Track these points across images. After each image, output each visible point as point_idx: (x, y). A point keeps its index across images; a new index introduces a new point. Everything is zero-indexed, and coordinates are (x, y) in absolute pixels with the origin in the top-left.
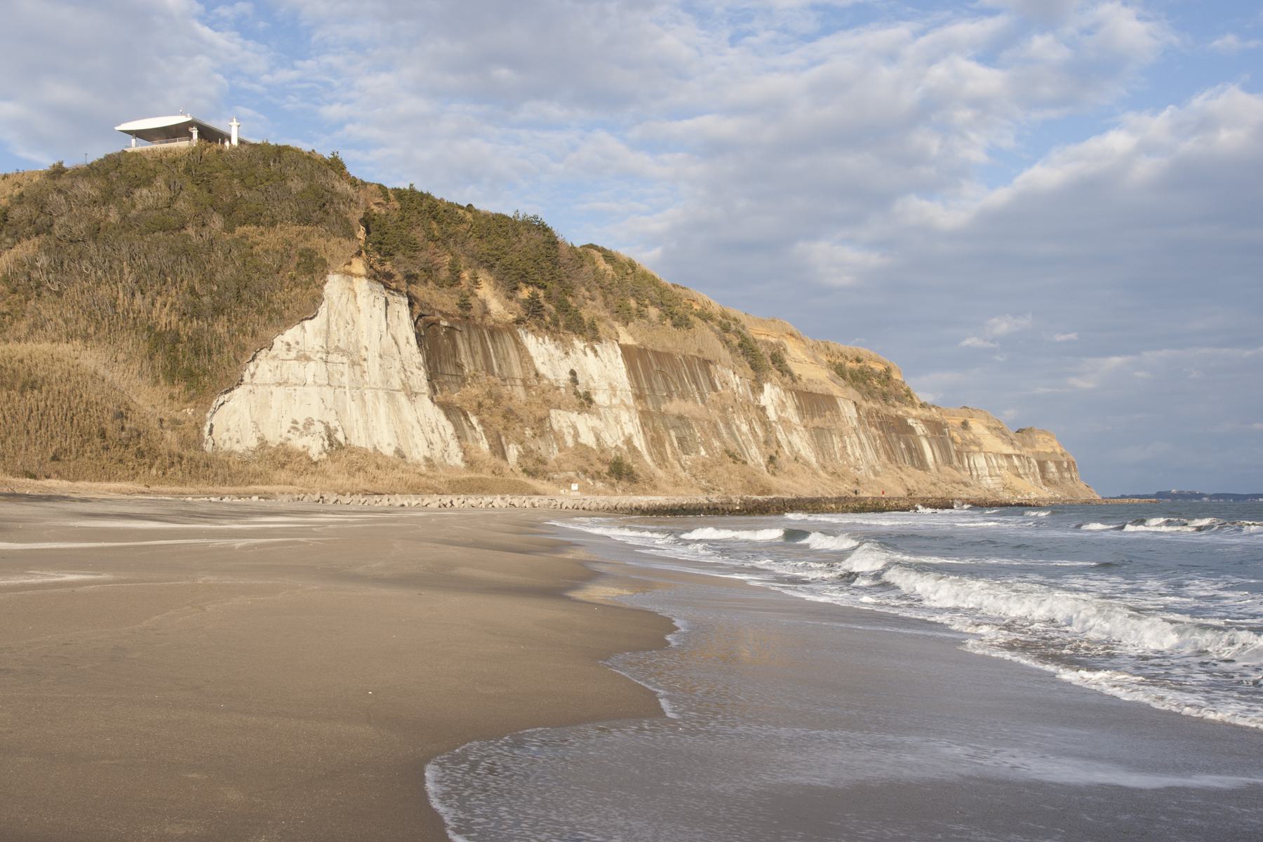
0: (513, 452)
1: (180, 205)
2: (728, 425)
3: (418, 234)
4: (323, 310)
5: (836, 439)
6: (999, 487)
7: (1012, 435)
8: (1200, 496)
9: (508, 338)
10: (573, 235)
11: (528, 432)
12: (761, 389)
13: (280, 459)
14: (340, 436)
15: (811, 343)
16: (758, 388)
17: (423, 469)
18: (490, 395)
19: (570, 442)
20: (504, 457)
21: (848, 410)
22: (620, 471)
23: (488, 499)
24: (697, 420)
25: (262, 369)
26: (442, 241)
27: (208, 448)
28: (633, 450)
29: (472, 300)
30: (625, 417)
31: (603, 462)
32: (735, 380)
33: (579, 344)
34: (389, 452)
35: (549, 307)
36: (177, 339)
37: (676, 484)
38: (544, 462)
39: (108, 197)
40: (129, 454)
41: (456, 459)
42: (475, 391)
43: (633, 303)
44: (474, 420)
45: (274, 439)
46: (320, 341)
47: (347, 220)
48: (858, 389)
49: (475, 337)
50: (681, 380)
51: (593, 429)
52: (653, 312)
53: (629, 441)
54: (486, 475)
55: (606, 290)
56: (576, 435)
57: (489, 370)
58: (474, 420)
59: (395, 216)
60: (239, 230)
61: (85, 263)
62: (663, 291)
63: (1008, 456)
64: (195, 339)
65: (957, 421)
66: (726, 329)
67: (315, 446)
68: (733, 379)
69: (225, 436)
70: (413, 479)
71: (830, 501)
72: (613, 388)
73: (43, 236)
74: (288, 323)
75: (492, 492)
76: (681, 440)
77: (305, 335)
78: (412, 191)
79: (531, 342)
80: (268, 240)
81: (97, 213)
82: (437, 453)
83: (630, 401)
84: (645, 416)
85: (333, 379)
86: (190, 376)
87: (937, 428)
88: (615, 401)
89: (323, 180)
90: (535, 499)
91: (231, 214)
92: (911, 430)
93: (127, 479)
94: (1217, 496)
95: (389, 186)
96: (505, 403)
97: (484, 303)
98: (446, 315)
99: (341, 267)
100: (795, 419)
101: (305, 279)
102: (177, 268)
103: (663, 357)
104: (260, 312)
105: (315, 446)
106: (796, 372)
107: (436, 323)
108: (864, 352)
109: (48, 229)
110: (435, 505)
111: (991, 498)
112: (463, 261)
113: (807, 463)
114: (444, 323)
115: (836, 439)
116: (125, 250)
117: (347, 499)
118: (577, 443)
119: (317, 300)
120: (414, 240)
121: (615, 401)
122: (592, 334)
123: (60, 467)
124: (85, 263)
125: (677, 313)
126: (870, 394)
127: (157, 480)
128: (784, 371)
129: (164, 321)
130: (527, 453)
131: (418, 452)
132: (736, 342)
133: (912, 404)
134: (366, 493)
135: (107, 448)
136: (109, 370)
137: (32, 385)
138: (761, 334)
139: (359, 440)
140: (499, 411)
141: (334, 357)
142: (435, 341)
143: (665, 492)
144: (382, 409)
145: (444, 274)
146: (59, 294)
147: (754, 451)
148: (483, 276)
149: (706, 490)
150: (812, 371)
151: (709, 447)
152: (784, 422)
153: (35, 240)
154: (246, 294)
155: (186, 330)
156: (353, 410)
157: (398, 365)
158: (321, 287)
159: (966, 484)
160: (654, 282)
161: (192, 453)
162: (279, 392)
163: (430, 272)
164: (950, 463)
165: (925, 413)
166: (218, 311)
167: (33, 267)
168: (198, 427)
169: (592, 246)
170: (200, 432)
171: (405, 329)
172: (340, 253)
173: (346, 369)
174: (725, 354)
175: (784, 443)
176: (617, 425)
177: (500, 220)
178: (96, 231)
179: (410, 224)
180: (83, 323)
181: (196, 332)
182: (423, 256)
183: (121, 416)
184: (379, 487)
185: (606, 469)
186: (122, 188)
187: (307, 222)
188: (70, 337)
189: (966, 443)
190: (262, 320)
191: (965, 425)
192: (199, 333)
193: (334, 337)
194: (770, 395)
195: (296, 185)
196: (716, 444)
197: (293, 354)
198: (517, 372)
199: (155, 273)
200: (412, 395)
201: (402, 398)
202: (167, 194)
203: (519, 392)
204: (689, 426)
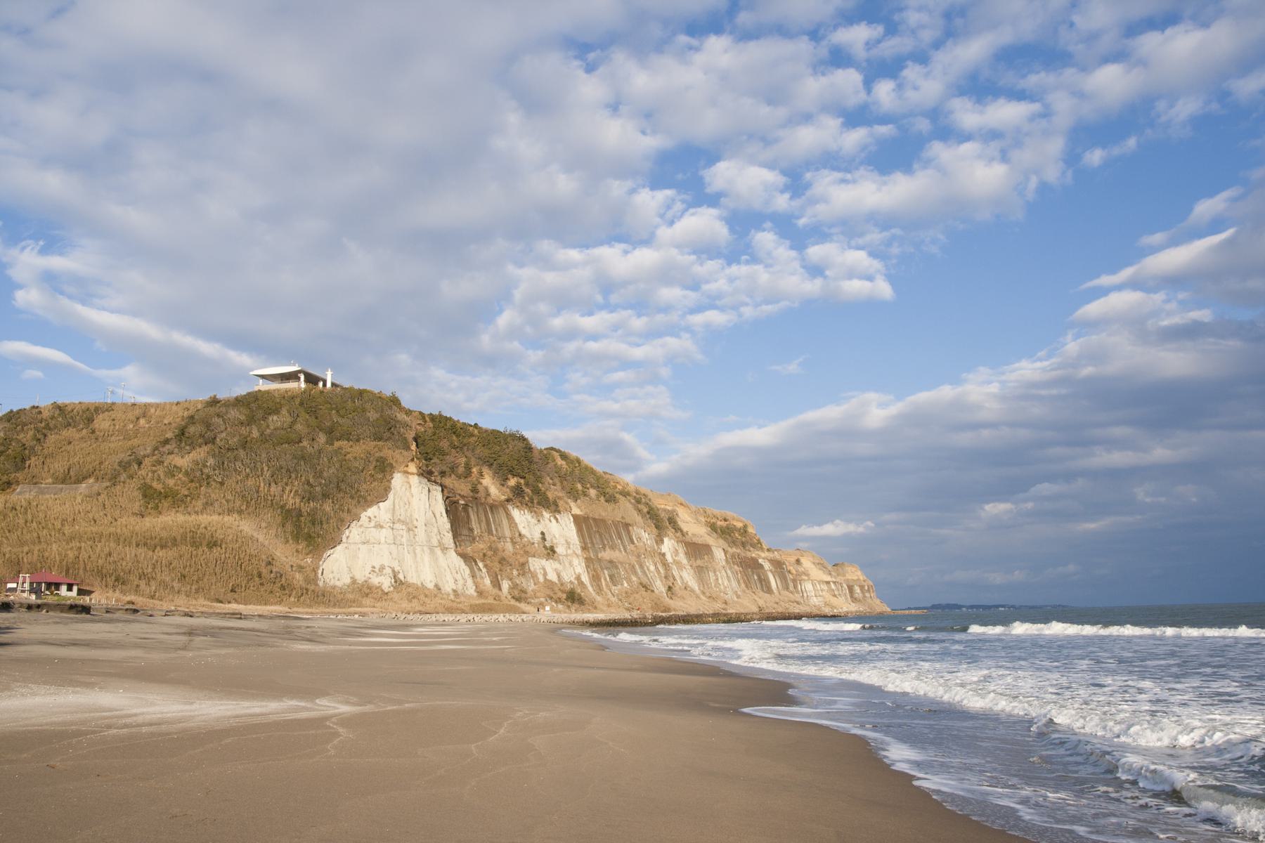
0: (505, 585)
1: (298, 427)
2: (641, 566)
3: (444, 444)
4: (391, 496)
5: (711, 574)
6: (822, 604)
7: (830, 567)
8: (960, 607)
10: (540, 438)
11: (515, 572)
12: (662, 541)
13: (365, 591)
14: (401, 576)
15: (694, 508)
16: (660, 541)
17: (452, 597)
18: (490, 548)
19: (541, 579)
20: (500, 589)
21: (719, 554)
22: (573, 597)
23: (495, 616)
24: (621, 563)
25: (353, 533)
26: (459, 448)
27: (321, 583)
28: (581, 583)
29: (479, 487)
30: (576, 562)
31: (563, 592)
32: (645, 536)
33: (546, 515)
34: (431, 586)
35: (528, 491)
36: (300, 514)
37: (609, 606)
38: (525, 592)
39: (251, 421)
40: (276, 588)
41: (471, 590)
42: (481, 546)
43: (579, 486)
44: (481, 565)
45: (360, 578)
46: (389, 516)
47: (405, 439)
48: (725, 539)
49: (481, 511)
50: (611, 537)
52: (593, 492)
53: (578, 578)
54: (490, 601)
55: (563, 478)
56: (545, 574)
57: (490, 532)
58: (481, 565)
59: (430, 432)
60: (337, 444)
61: (238, 464)
62: (598, 478)
63: (828, 583)
65: (793, 559)
66: (639, 502)
67: (386, 583)
68: (644, 535)
69: (331, 576)
70: (449, 604)
71: (708, 616)
72: (568, 543)
73: (209, 445)
74: (368, 503)
75: (496, 612)
76: (611, 577)
78: (440, 415)
79: (516, 513)
80: (355, 451)
81: (244, 431)
82: (460, 587)
83: (579, 552)
85: (397, 539)
86: (309, 538)
87: (778, 564)
88: (570, 552)
89: (389, 412)
90: (524, 616)
91: (332, 433)
92: (761, 566)
93: (276, 604)
94: (972, 607)
95: (426, 412)
97: (486, 489)
98: (463, 497)
99: (402, 468)
100: (685, 561)
101: (380, 476)
103: (600, 522)
104: (352, 498)
105: (386, 583)
106: (685, 530)
107: (457, 502)
108: (729, 514)
109: (213, 441)
110: (463, 621)
111: (815, 611)
113: (693, 591)
114: (462, 502)
115: (711, 574)
116: (264, 455)
117: (411, 617)
118: (545, 579)
119: (387, 490)
120: (448, 449)
121: (570, 552)
122: (554, 507)
123: (236, 596)
124: (238, 464)
125: (607, 490)
126: (733, 543)
127: (294, 604)
128: (677, 529)
129: (291, 501)
130: (514, 586)
131: (448, 587)
132: (645, 510)
133: (762, 549)
134: (421, 613)
135: (262, 584)
136: (257, 533)
137: (213, 544)
138: (662, 504)
139: (413, 578)
140: (496, 559)
141: (397, 526)
142: (457, 513)
143: (602, 611)
144: (426, 558)
145: (461, 469)
146: (222, 484)
147: (658, 583)
148: (486, 470)
149: (628, 609)
150: (695, 528)
151: (629, 581)
152: (678, 563)
153: (206, 448)
154: (343, 486)
155: (306, 509)
156: (408, 558)
157: (435, 530)
158: (389, 481)
159: (798, 603)
160: (593, 472)
161: (312, 587)
163: (453, 469)
164: (787, 588)
165: (770, 555)
166: (325, 496)
167: (205, 466)
168: (315, 570)
169: (552, 449)
170: (316, 574)
171: (440, 507)
172: (401, 460)
174: (639, 519)
175: (677, 578)
176: (571, 567)
177: (495, 433)
178: (244, 444)
179: (439, 438)
180: (238, 503)
181: (312, 510)
182: (449, 459)
183: (269, 563)
184: (428, 608)
185: (564, 596)
186: (260, 414)
187: (380, 439)
188: (230, 511)
189: (799, 574)
190: (354, 502)
191: (798, 561)
192: (314, 510)
193: (398, 513)
194: (668, 545)
195: (372, 415)
196: (634, 579)
197: (373, 524)
198: (507, 533)
199: (284, 471)
200: (444, 549)
201: (438, 552)
202: (289, 420)
203: (509, 546)
204: (617, 567)
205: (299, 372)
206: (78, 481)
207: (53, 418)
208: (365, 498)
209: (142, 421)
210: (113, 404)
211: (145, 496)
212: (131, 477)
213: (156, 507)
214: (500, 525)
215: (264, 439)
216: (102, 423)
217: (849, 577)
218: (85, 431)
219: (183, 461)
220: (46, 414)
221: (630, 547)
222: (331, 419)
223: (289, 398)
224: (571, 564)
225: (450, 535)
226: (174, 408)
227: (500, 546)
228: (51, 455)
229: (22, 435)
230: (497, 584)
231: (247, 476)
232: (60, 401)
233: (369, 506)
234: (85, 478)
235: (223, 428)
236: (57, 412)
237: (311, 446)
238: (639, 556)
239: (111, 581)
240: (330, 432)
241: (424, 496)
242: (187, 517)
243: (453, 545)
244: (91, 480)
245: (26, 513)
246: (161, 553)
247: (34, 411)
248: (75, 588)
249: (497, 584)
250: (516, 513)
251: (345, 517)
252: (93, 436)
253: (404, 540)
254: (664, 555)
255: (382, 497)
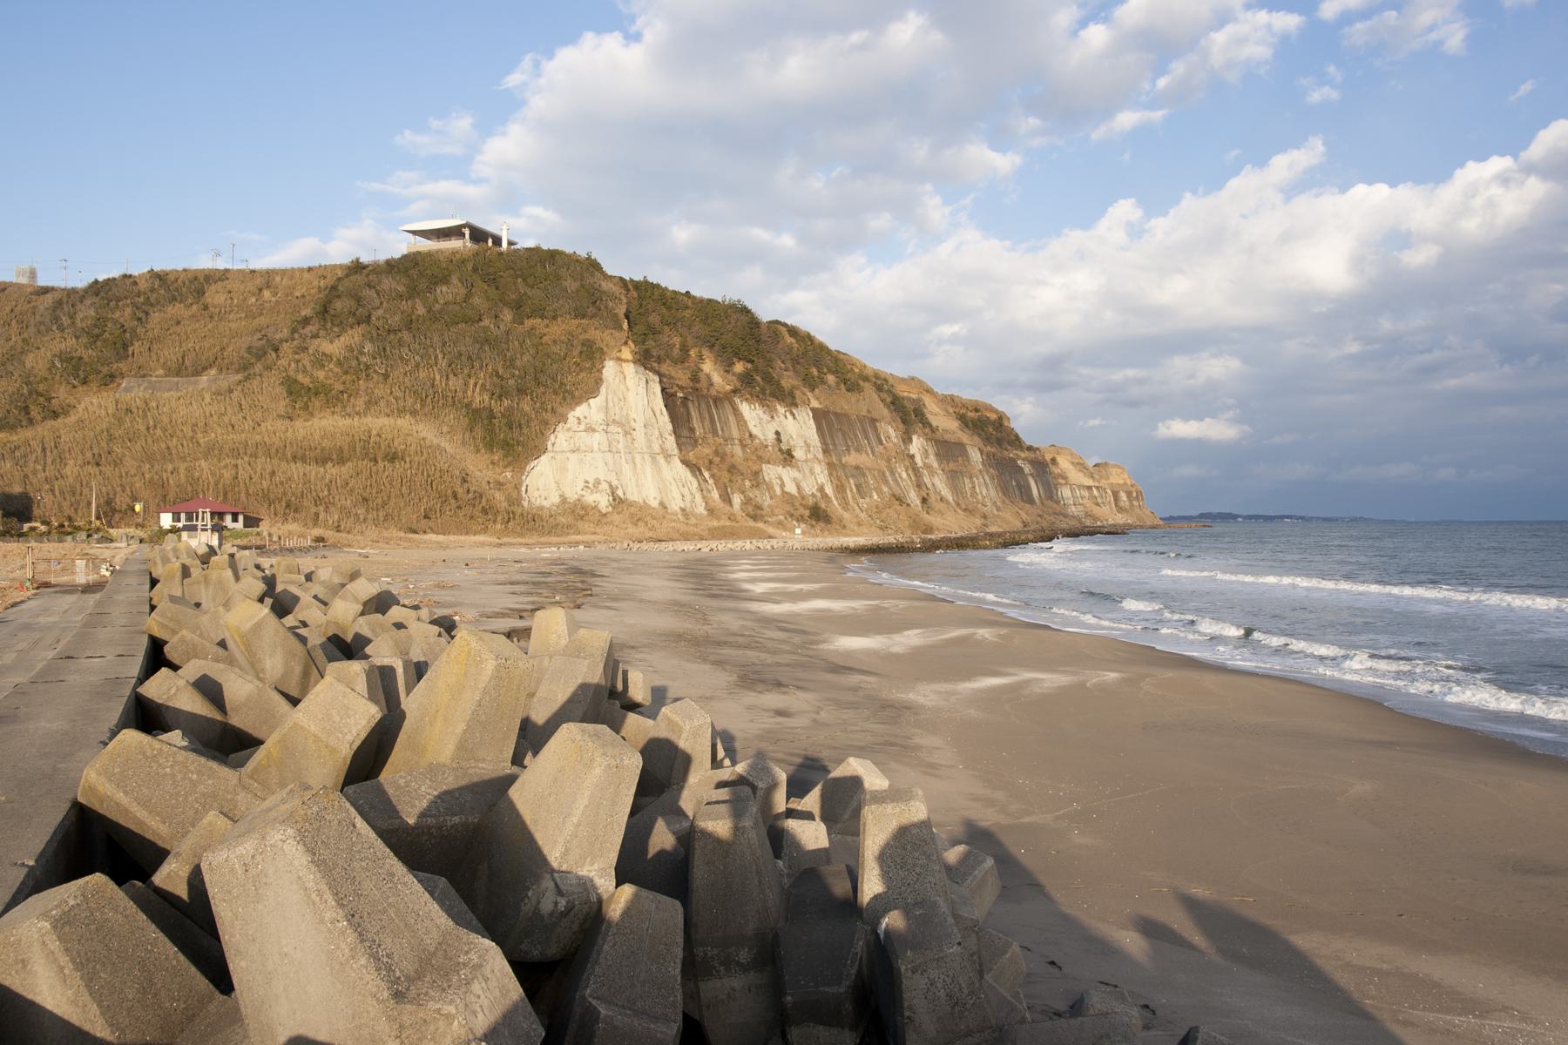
0: (737, 499)
1: (476, 300)
2: (892, 473)
4: (603, 390)
6: (1082, 515)
9: (727, 405)
11: (747, 483)
12: (911, 440)
13: (578, 513)
14: (620, 493)
16: (907, 440)
18: (716, 453)
19: (778, 492)
21: (975, 456)
23: (740, 543)
25: (560, 439)
27: (525, 504)
30: (817, 469)
31: (805, 507)
33: (781, 409)
34: (654, 504)
36: (492, 416)
39: (413, 292)
40: (477, 512)
41: (701, 509)
42: (706, 451)
43: (815, 371)
44: (706, 474)
45: (572, 496)
46: (602, 416)
49: (703, 405)
51: (794, 479)
52: (831, 378)
53: (821, 489)
56: (782, 485)
57: (715, 433)
58: (706, 474)
60: (529, 323)
63: (1089, 488)
64: (508, 414)
67: (603, 501)
68: (890, 431)
69: (536, 494)
72: (807, 445)
74: (578, 401)
75: (739, 538)
76: (858, 487)
77: (589, 411)
78: (646, 282)
79: (745, 408)
80: (555, 331)
81: (404, 305)
83: (821, 456)
84: (830, 466)
85: (609, 445)
86: (507, 446)
90: (774, 542)
91: (519, 307)
96: (729, 460)
97: (708, 376)
98: (681, 388)
99: (614, 355)
100: (935, 465)
102: (483, 355)
103: (841, 417)
104: (555, 393)
105: (603, 501)
106: (934, 424)
107: (674, 395)
112: (690, 341)
113: (948, 503)
115: (967, 481)
119: (599, 382)
120: (662, 324)
128: (926, 423)
130: (747, 501)
131: (675, 505)
134: (651, 540)
135: (459, 508)
136: (436, 438)
137: (393, 457)
139: (633, 495)
140: (725, 466)
141: (612, 428)
144: (648, 470)
145: (676, 351)
146: (386, 376)
148: (706, 352)
151: (880, 492)
152: (928, 466)
153: (360, 330)
154: (543, 379)
157: (656, 433)
158: (600, 371)
162: (574, 457)
166: (521, 391)
167: (362, 353)
168: (517, 487)
169: (777, 322)
173: (621, 437)
174: (886, 412)
176: (809, 477)
178: (409, 324)
180: (410, 401)
181: (507, 409)
185: (807, 513)
186: (423, 284)
187: (584, 317)
188: (401, 412)
192: (510, 409)
194: (917, 445)
195: (571, 285)
197: (582, 427)
198: (735, 433)
200: (668, 457)
201: (661, 460)
202: (463, 291)
203: (738, 450)
204: (864, 475)
205: (464, 226)
206: (197, 373)
207: (152, 290)
208: (572, 394)
209: (267, 294)
210: (227, 271)
211: (290, 393)
212: (269, 368)
213: (306, 408)
214: (725, 423)
215: (433, 317)
216: (216, 296)
217: (1113, 480)
218: (195, 307)
219: (333, 348)
220: (143, 286)
221: (879, 449)
222: (517, 290)
223: (456, 262)
224: (812, 472)
225: (672, 439)
226: (306, 275)
227: (728, 449)
228: (158, 339)
229: (118, 314)
230: (727, 499)
231: (418, 365)
232: (157, 268)
233: (578, 404)
234: (205, 369)
235: (377, 302)
236: (157, 283)
237: (494, 324)
238: (889, 461)
239: (281, 508)
240: (517, 306)
241: (642, 391)
242: (348, 421)
243: (676, 451)
244: (213, 372)
245: (145, 416)
246: (332, 470)
247: (128, 282)
248: (241, 518)
249: (727, 499)
250: (745, 408)
251: (550, 418)
252: (205, 313)
253: (621, 446)
254: (912, 457)
255: (593, 391)
